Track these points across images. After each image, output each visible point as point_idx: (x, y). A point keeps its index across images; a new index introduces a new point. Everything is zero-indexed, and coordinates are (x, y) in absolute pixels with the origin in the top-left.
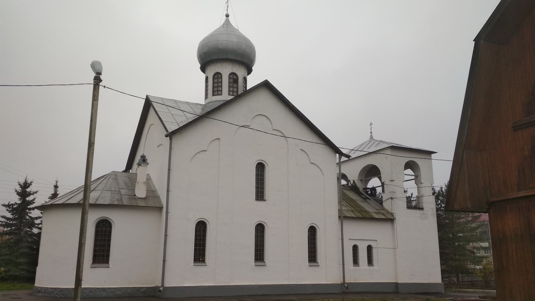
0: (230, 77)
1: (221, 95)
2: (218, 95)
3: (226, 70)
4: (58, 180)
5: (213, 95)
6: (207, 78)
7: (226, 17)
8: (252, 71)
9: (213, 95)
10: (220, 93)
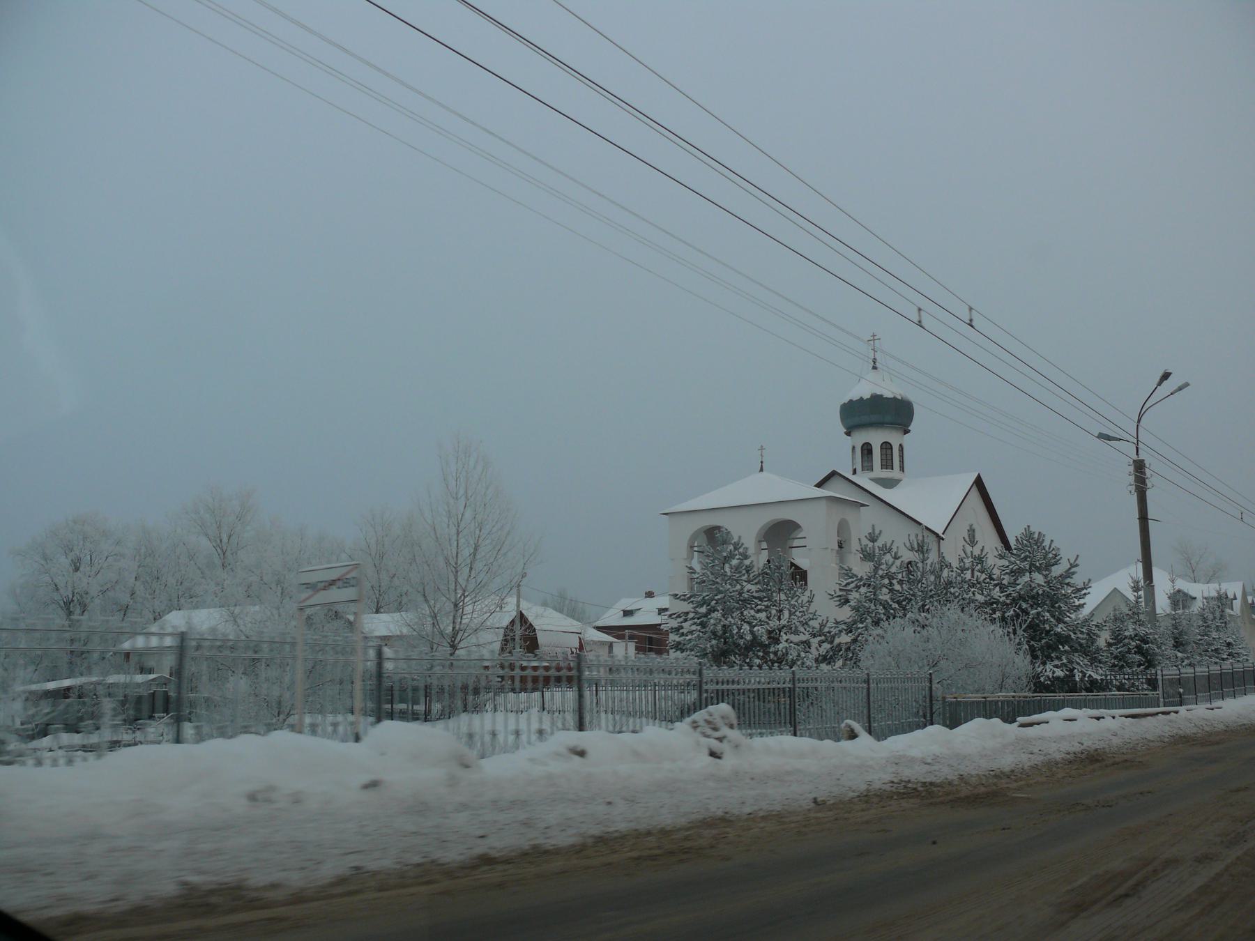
0: (864, 448)
3: (876, 438)
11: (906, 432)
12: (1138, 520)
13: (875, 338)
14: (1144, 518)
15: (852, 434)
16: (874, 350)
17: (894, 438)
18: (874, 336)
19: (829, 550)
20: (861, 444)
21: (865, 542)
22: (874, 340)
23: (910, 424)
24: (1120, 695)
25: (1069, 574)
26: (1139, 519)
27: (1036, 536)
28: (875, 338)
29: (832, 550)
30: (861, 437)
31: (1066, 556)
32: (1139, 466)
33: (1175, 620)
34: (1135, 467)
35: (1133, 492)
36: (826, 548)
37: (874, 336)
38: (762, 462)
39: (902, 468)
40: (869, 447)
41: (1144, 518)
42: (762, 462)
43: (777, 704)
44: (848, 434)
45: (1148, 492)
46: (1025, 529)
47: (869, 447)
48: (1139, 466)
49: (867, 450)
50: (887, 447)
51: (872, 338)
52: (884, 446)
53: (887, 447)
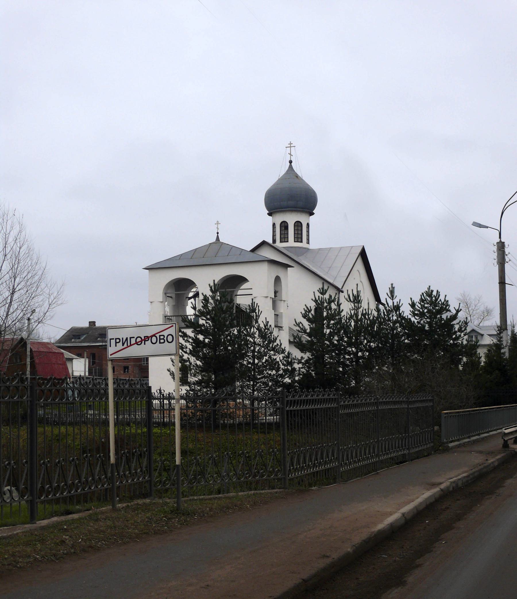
0: (282, 225)
1: (288, 242)
2: (285, 242)
3: (291, 219)
4: (204, 295)
5: (302, 242)
6: (274, 225)
7: (289, 164)
8: (314, 193)
9: (302, 242)
10: (286, 240)
11: (312, 214)
12: (498, 284)
13: (292, 145)
14: (502, 283)
15: (273, 215)
16: (290, 154)
17: (303, 218)
18: (291, 144)
19: (269, 298)
20: (303, 224)
21: (318, 294)
22: (290, 147)
23: (314, 209)
24: (415, 402)
25: (454, 317)
26: (499, 283)
27: (434, 293)
28: (292, 145)
29: (270, 298)
30: (279, 218)
31: (453, 306)
32: (501, 246)
33: (301, 362)
34: (498, 246)
35: (496, 263)
36: (267, 297)
37: (291, 144)
38: (218, 233)
39: (308, 243)
40: (286, 225)
41: (502, 283)
42: (218, 233)
43: (81, 410)
44: (270, 214)
45: (506, 265)
46: (428, 288)
47: (299, 224)
48: (501, 246)
49: (284, 226)
50: (298, 225)
51: (289, 146)
52: (283, 224)
53: (298, 225)
